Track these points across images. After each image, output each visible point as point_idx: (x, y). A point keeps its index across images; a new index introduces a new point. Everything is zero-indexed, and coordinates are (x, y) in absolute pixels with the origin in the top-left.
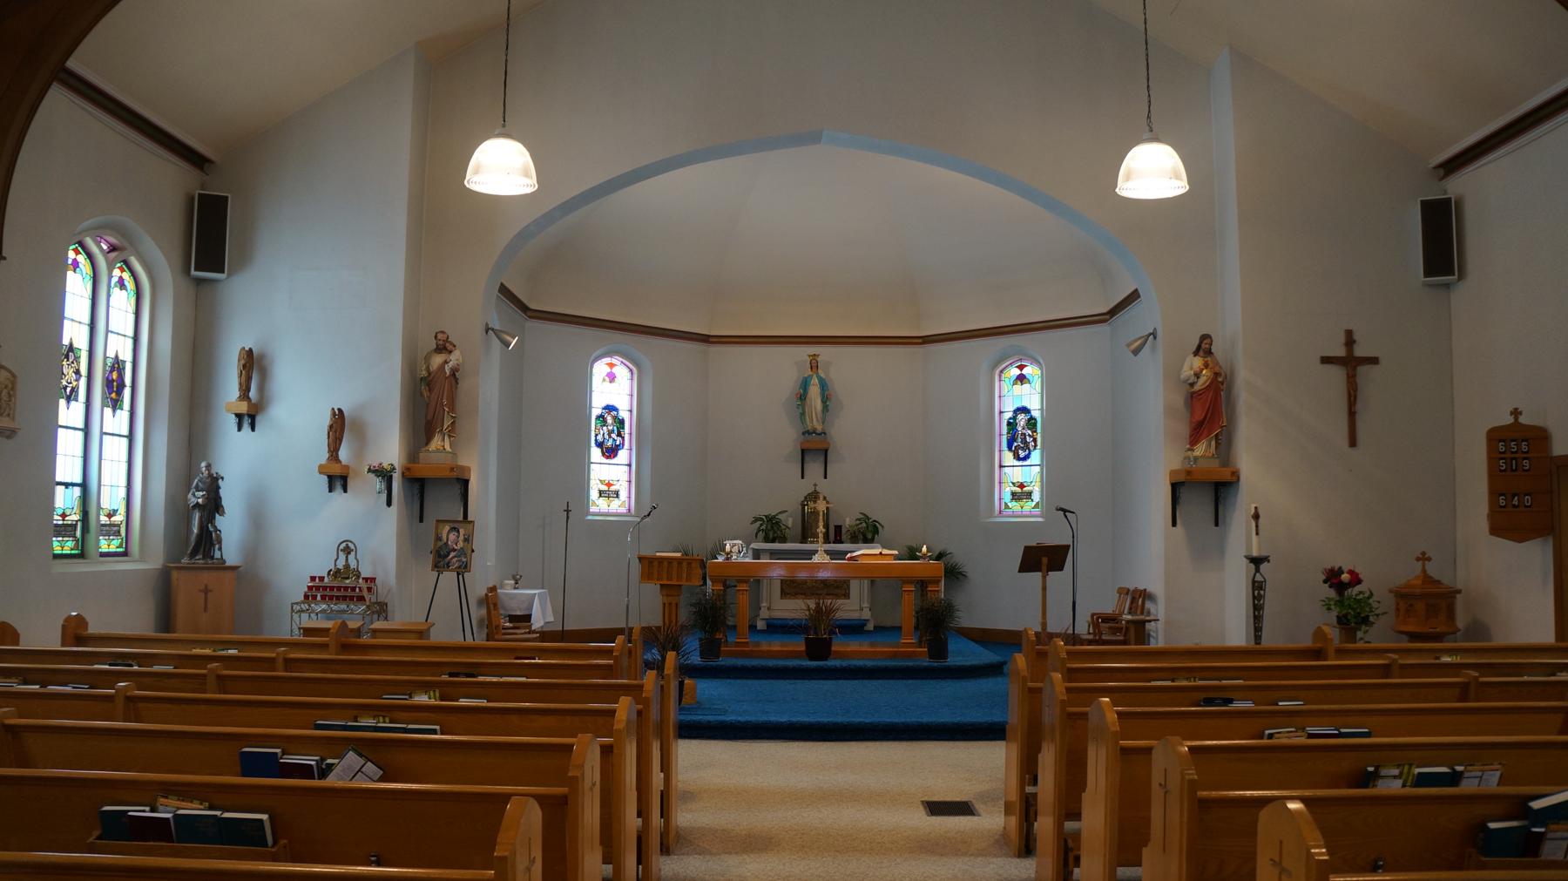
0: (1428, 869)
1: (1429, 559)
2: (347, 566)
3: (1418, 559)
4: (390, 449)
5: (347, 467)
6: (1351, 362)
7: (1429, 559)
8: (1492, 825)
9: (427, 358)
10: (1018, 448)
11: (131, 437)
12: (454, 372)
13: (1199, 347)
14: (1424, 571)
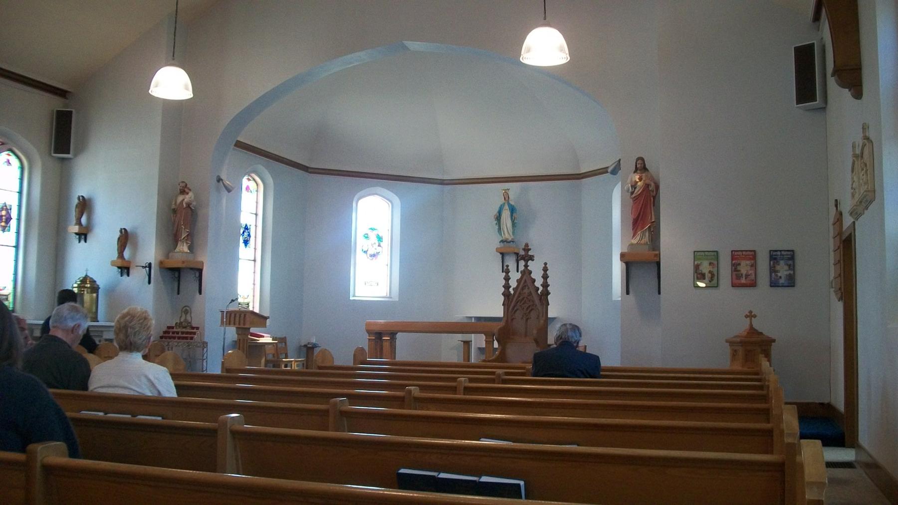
0: (115, 461)
1: (755, 316)
2: (186, 320)
3: (747, 316)
4: (149, 251)
5: (129, 262)
7: (755, 316)
8: (402, 471)
9: (177, 197)
11: (17, 247)
12: (188, 205)
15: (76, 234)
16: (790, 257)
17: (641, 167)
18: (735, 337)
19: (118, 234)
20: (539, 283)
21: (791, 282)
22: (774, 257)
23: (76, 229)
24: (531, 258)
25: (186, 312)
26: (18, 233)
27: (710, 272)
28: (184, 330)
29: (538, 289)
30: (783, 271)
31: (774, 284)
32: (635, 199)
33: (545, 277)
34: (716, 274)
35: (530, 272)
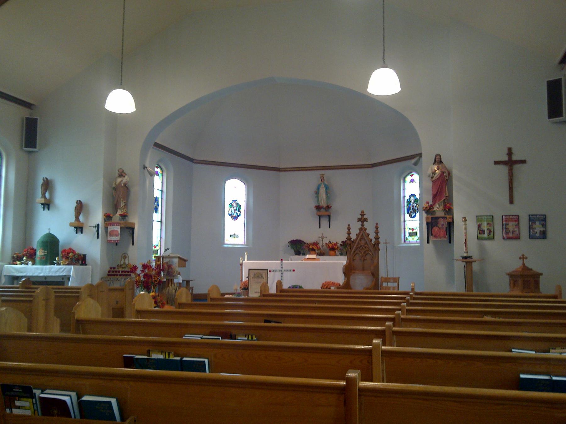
1: (526, 258)
2: (124, 263)
3: (520, 258)
4: (98, 218)
5: (83, 224)
6: (510, 162)
8: (522, 376)
9: (116, 179)
10: (411, 212)
12: (125, 185)
13: (435, 160)
14: (524, 264)
15: (42, 204)
16: (543, 219)
17: (438, 160)
18: (514, 271)
19: (75, 204)
20: (372, 236)
21: (544, 235)
22: (532, 219)
23: (43, 201)
24: (366, 220)
25: (125, 257)
26: (161, 214)
27: (488, 229)
28: (124, 270)
29: (371, 240)
30: (538, 228)
31: (532, 237)
32: (434, 182)
33: (377, 233)
34: (492, 230)
35: (366, 229)
